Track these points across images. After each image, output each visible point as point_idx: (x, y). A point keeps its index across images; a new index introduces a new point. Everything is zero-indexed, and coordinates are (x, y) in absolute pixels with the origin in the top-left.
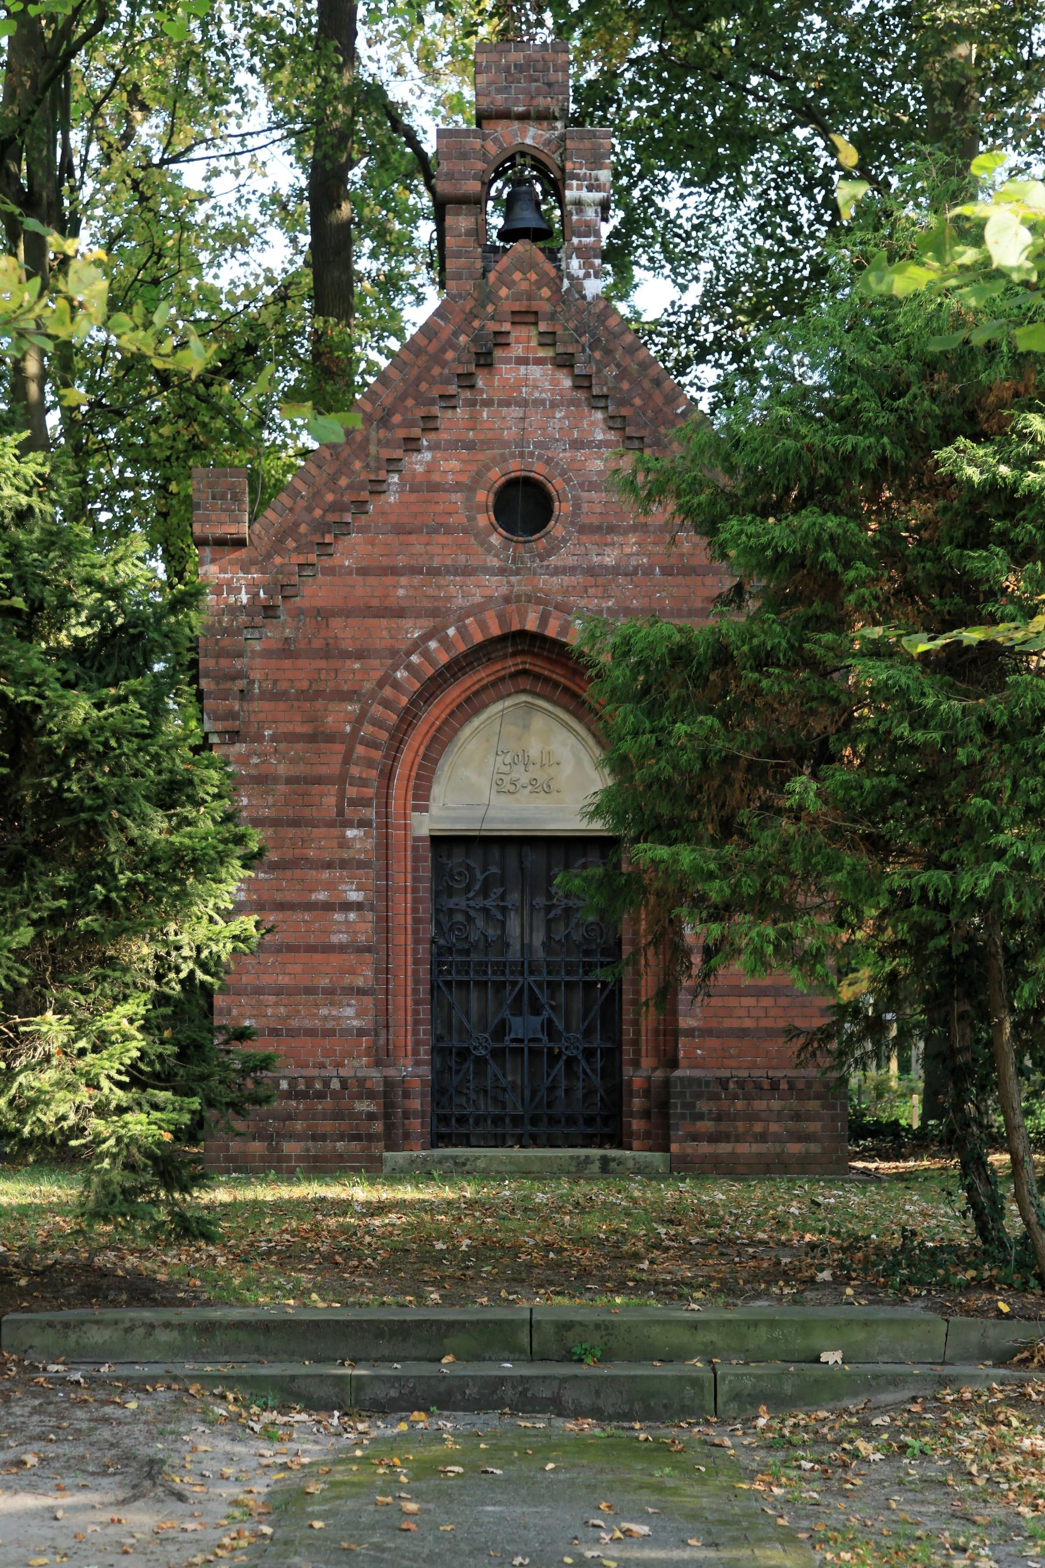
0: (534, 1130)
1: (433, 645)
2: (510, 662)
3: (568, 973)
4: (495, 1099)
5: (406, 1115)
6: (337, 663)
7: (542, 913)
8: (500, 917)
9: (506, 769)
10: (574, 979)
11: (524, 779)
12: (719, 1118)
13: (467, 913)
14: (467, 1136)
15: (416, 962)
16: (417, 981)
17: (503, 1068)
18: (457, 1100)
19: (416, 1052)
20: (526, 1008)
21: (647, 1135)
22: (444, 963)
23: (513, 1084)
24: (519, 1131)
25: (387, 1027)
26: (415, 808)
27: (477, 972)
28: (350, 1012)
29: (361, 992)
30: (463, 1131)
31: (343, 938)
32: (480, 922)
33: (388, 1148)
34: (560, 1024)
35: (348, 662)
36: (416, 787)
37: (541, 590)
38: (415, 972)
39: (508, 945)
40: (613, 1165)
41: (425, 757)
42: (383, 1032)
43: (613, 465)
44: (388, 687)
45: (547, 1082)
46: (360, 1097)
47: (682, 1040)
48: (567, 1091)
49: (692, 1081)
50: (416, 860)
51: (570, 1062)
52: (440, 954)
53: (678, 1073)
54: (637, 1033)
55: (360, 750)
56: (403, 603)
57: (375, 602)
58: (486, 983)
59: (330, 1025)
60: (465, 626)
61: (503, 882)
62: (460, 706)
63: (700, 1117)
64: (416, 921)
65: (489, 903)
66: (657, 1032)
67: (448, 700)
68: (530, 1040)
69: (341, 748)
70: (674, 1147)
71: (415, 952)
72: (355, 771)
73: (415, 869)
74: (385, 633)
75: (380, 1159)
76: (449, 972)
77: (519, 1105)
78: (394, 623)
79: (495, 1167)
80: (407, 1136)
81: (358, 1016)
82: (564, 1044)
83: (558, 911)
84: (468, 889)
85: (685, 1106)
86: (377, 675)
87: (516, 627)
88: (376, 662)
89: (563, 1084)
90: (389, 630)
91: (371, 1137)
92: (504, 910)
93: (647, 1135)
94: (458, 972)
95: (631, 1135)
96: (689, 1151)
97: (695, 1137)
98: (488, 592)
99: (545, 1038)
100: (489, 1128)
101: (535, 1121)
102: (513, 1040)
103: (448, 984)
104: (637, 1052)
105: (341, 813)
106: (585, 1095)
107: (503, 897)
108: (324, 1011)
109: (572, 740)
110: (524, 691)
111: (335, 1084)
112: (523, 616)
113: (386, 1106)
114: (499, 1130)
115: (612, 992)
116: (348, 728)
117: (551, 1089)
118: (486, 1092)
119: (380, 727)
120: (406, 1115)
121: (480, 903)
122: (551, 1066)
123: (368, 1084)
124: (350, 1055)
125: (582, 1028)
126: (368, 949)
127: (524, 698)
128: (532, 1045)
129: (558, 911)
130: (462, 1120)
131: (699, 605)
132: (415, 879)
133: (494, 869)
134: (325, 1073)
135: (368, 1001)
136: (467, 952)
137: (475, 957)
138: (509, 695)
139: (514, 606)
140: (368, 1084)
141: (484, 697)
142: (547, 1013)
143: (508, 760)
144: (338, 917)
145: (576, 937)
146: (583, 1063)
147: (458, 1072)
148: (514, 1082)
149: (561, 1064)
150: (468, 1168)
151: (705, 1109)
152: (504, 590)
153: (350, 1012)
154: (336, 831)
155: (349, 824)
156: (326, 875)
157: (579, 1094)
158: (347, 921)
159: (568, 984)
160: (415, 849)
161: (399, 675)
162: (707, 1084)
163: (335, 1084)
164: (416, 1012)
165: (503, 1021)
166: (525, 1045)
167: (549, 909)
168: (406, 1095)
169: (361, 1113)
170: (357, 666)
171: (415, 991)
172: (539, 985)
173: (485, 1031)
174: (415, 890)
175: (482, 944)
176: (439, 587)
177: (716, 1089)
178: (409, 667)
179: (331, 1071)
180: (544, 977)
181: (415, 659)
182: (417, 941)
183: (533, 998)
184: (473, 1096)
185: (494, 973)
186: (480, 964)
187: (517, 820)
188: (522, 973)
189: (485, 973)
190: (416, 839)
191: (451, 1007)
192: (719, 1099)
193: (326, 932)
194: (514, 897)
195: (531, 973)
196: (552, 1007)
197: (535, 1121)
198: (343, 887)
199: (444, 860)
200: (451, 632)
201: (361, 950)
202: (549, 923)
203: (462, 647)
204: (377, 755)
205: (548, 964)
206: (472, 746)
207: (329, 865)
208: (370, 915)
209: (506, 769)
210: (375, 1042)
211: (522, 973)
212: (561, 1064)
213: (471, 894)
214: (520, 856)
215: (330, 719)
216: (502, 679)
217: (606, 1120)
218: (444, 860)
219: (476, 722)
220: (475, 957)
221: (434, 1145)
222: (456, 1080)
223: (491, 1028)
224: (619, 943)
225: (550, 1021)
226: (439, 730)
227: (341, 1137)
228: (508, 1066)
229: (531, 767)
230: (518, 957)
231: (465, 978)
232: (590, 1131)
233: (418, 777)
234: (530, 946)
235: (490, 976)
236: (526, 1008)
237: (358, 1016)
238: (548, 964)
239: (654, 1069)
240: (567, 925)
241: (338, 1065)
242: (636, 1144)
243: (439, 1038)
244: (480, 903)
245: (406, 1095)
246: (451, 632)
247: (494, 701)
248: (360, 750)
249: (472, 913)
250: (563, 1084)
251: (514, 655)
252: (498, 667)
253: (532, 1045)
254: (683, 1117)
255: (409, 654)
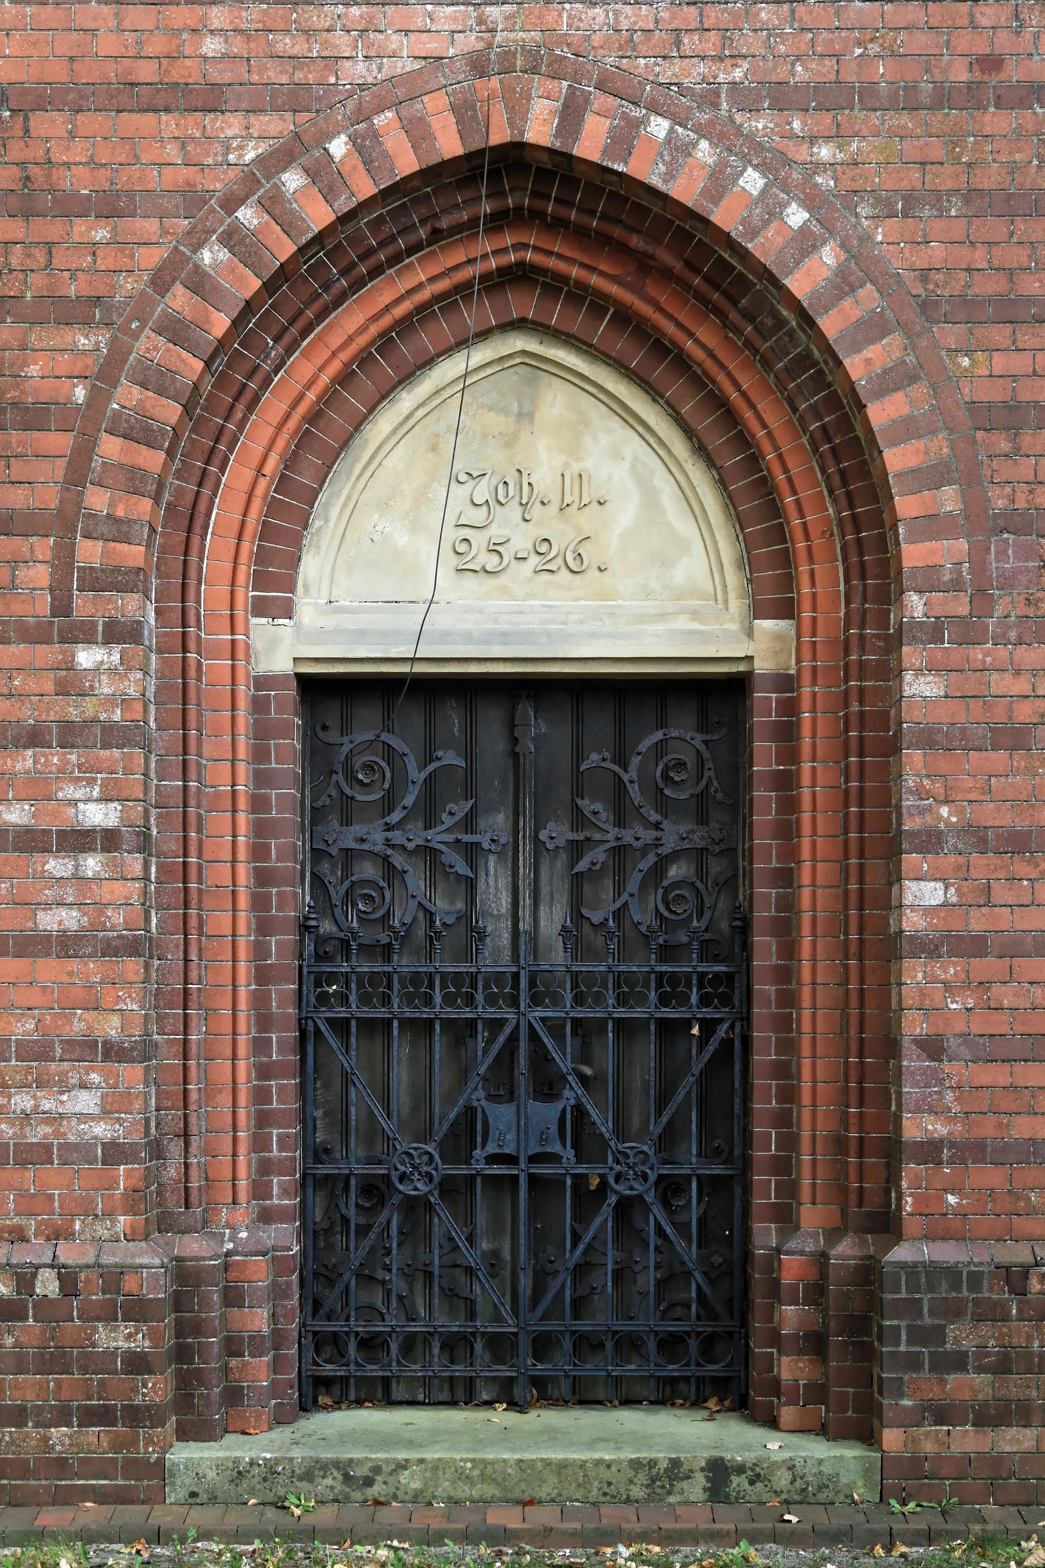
0: (542, 1368)
1: (292, 180)
2: (485, 245)
3: (622, 1000)
4: (451, 1294)
5: (233, 1347)
6: (52, 229)
7: (563, 858)
8: (463, 869)
9: (478, 516)
10: (638, 1013)
11: (521, 541)
12: (1002, 1366)
13: (386, 859)
14: (386, 1382)
15: (263, 976)
16: (264, 1021)
17: (469, 1219)
18: (361, 1296)
19: (260, 1190)
20: (523, 1083)
21: (817, 1393)
22: (332, 978)
23: (493, 1260)
24: (504, 1371)
25: (186, 1135)
26: (260, 608)
27: (408, 999)
28: (86, 1102)
29: (113, 1052)
30: (373, 1370)
31: (70, 919)
32: (417, 881)
33: (184, 1434)
34: (602, 1120)
35: (80, 227)
36: (262, 556)
37: (564, 40)
38: (259, 1000)
39: (482, 935)
40: (738, 1482)
41: (283, 483)
42: (175, 1149)
43: (402, 1488)
44: (178, 289)
45: (573, 1257)
46: (109, 1316)
47: (910, 1172)
48: (618, 1275)
49: (935, 1272)
50: (261, 732)
51: (625, 1208)
52: (321, 957)
53: (901, 1253)
54: (790, 1142)
55: (110, 447)
56: (217, 74)
57: (146, 72)
58: (430, 1023)
59: (38, 1134)
60: (375, 135)
61: (469, 789)
62: (364, 359)
63: (958, 1362)
64: (263, 877)
65: (438, 837)
66: (840, 1144)
67: (336, 340)
68: (532, 1159)
69: (62, 442)
70: (892, 1438)
71: (260, 951)
72: (97, 500)
73: (260, 754)
74: (172, 151)
75: (159, 1470)
76: (344, 1000)
77: (506, 1312)
78: (192, 125)
79: (445, 1487)
80: (234, 1396)
81: (106, 1112)
82: (612, 1167)
83: (599, 855)
84: (389, 803)
85: (917, 1335)
86: (151, 258)
87: (499, 135)
88: (151, 226)
89: (611, 1257)
90: (183, 142)
91: (136, 1416)
92: (472, 852)
93: (817, 1393)
94: (365, 999)
95: (775, 1387)
96: (929, 1447)
97: (943, 1414)
98: (431, 46)
99: (569, 1154)
100: (438, 1364)
101: (542, 1346)
102: (492, 1159)
103: (341, 1026)
104: (790, 1189)
105: (62, 607)
106: (660, 1284)
107: (469, 823)
108: (22, 1101)
109: (633, 445)
110: (520, 325)
111: (48, 1285)
112: (518, 111)
113: (181, 1330)
114: (459, 1370)
115: (727, 1044)
116: (80, 394)
117: (582, 1270)
118: (429, 1275)
119: (160, 392)
120: (233, 1347)
121: (416, 835)
122: (582, 1217)
123: (129, 1284)
124: (88, 1212)
125: (655, 1129)
126: (132, 947)
127: (518, 342)
128: (537, 1170)
129: (599, 855)
130: (371, 1344)
131: (961, 74)
132: (261, 779)
133: (450, 758)
134: (22, 1255)
135: (131, 1074)
136: (386, 952)
137: (404, 963)
138: (484, 335)
139: (495, 82)
140: (129, 1284)
141: (425, 339)
142: (572, 1093)
143: (482, 492)
144: (57, 866)
145: (643, 915)
146: (657, 1212)
147: (363, 1231)
148: (495, 1253)
149: (604, 1216)
150: (377, 1489)
151: (968, 1344)
152: (470, 42)
153: (86, 1102)
154: (49, 653)
155: (84, 634)
156: (26, 761)
157: (648, 1279)
158: (78, 878)
159: (621, 1025)
160: (259, 705)
161: (206, 256)
162: (975, 1280)
163: (48, 1285)
164: (261, 1095)
165: (470, 1112)
166: (521, 1171)
167: (577, 850)
168: (233, 1298)
169: (111, 1354)
170: (101, 234)
171: (260, 1045)
172: (555, 1028)
173: (425, 1135)
174: (258, 804)
175: (420, 932)
176: (308, 32)
177: (994, 1292)
178: (233, 238)
179: (36, 1251)
180: (567, 1009)
181: (247, 215)
182: (264, 927)
183: (540, 1058)
184: (398, 1284)
185: (449, 1000)
186: (416, 978)
187: (504, 637)
188: (514, 1002)
189: (428, 1000)
190: (263, 682)
191: (347, 1079)
192: (1006, 1318)
193: (30, 905)
194: (500, 820)
195: (536, 1000)
196: (583, 1079)
197: (542, 1346)
198: (69, 791)
199: (333, 736)
200: (338, 147)
201: (112, 949)
202: (577, 881)
203: (365, 188)
204: (153, 460)
205: (576, 978)
206: (395, 461)
207: (35, 738)
208: (134, 863)
209: (478, 516)
210: (149, 1177)
211: (514, 1002)
212: (604, 1216)
213: (395, 817)
214: (511, 725)
215: (34, 370)
216: (463, 290)
217: (708, 1346)
218: (333, 736)
219: (407, 400)
220: (404, 963)
221: (307, 1406)
222: (357, 1255)
223: (441, 1130)
224: (744, 929)
225: (579, 1111)
226: (314, 417)
227: (62, 1417)
228: (481, 1218)
229: (536, 510)
230: (505, 964)
231: (381, 1013)
232: (673, 1369)
233: (267, 532)
234: (534, 936)
235: (440, 1009)
236: (523, 1083)
237: (106, 1112)
238: (576, 978)
239: (834, 1235)
240: (619, 892)
241: (58, 1234)
242: (787, 1414)
243: (316, 1153)
244: (416, 835)
245: (233, 1298)
246: (338, 147)
247: (448, 351)
248: (110, 447)
249: (398, 860)
250: (611, 1257)
251: (498, 222)
252: (459, 256)
253: (537, 1170)
254: (913, 1363)
255: (231, 204)
